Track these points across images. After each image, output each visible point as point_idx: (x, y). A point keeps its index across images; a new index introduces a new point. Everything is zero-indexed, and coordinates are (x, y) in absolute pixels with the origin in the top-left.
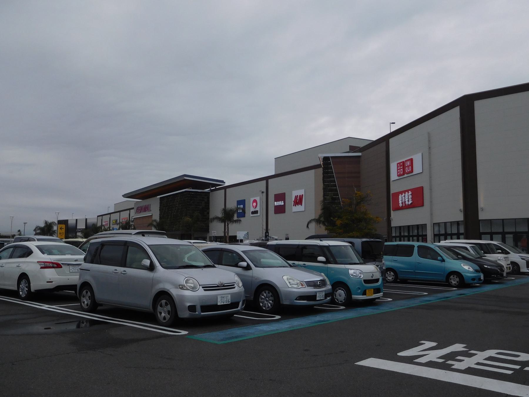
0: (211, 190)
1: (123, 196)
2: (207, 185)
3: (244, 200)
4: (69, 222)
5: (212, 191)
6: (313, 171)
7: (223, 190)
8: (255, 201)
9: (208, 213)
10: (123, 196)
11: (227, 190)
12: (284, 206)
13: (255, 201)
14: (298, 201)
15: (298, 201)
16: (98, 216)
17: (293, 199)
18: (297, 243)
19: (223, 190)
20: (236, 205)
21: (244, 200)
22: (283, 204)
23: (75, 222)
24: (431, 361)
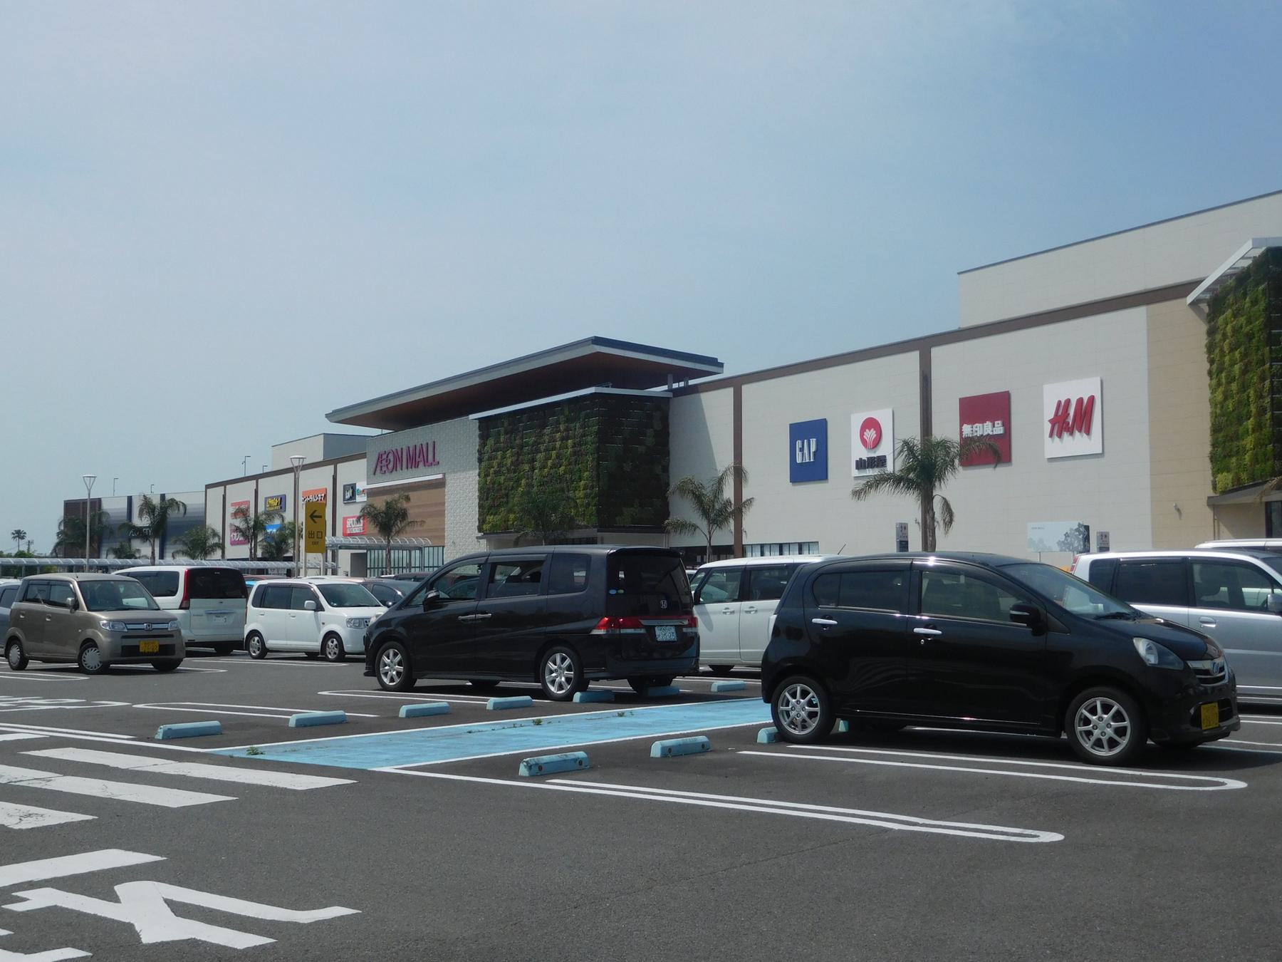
0: (670, 390)
1: (327, 416)
2: (657, 374)
3: (823, 423)
4: (106, 506)
5: (678, 393)
6: (1139, 314)
7: (730, 391)
8: (871, 424)
9: (666, 469)
10: (327, 416)
11: (745, 388)
12: (1006, 437)
13: (871, 424)
14: (1073, 419)
15: (1073, 419)
16: (208, 487)
17: (1050, 413)
18: (511, 604)
19: (730, 391)
20: (449, 479)
21: (823, 423)
22: (999, 429)
23: (125, 505)
24: (130, 927)
